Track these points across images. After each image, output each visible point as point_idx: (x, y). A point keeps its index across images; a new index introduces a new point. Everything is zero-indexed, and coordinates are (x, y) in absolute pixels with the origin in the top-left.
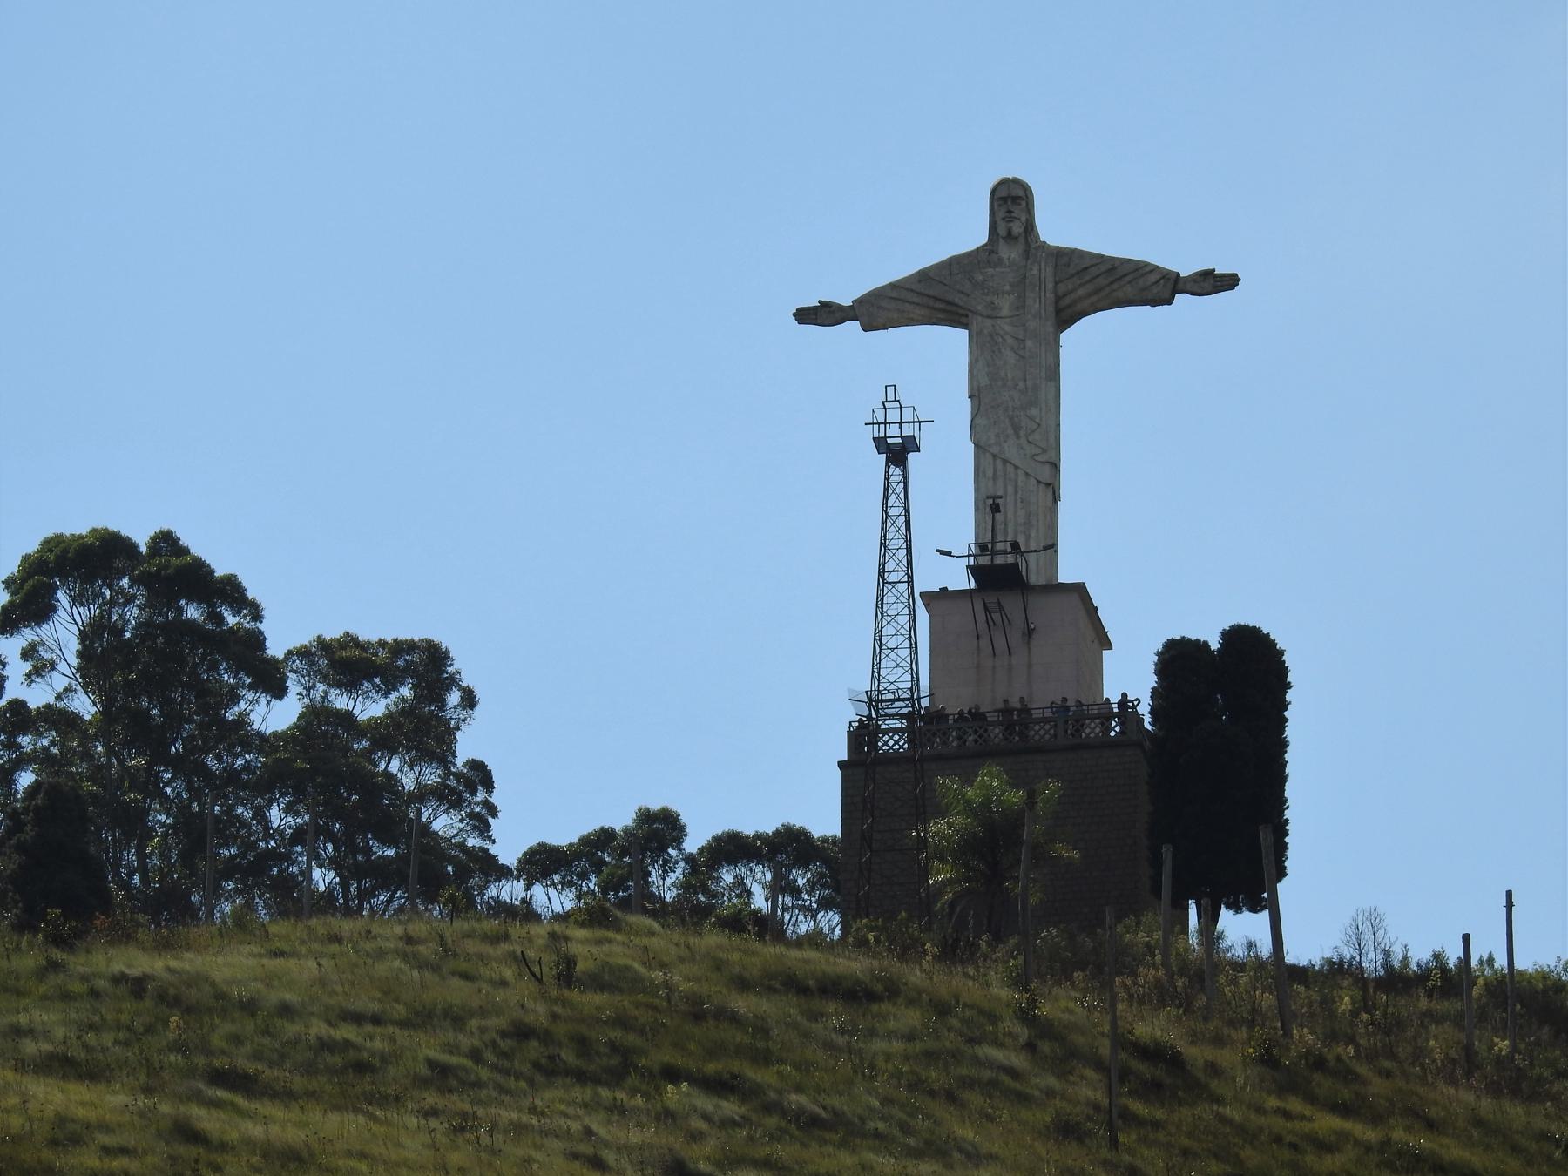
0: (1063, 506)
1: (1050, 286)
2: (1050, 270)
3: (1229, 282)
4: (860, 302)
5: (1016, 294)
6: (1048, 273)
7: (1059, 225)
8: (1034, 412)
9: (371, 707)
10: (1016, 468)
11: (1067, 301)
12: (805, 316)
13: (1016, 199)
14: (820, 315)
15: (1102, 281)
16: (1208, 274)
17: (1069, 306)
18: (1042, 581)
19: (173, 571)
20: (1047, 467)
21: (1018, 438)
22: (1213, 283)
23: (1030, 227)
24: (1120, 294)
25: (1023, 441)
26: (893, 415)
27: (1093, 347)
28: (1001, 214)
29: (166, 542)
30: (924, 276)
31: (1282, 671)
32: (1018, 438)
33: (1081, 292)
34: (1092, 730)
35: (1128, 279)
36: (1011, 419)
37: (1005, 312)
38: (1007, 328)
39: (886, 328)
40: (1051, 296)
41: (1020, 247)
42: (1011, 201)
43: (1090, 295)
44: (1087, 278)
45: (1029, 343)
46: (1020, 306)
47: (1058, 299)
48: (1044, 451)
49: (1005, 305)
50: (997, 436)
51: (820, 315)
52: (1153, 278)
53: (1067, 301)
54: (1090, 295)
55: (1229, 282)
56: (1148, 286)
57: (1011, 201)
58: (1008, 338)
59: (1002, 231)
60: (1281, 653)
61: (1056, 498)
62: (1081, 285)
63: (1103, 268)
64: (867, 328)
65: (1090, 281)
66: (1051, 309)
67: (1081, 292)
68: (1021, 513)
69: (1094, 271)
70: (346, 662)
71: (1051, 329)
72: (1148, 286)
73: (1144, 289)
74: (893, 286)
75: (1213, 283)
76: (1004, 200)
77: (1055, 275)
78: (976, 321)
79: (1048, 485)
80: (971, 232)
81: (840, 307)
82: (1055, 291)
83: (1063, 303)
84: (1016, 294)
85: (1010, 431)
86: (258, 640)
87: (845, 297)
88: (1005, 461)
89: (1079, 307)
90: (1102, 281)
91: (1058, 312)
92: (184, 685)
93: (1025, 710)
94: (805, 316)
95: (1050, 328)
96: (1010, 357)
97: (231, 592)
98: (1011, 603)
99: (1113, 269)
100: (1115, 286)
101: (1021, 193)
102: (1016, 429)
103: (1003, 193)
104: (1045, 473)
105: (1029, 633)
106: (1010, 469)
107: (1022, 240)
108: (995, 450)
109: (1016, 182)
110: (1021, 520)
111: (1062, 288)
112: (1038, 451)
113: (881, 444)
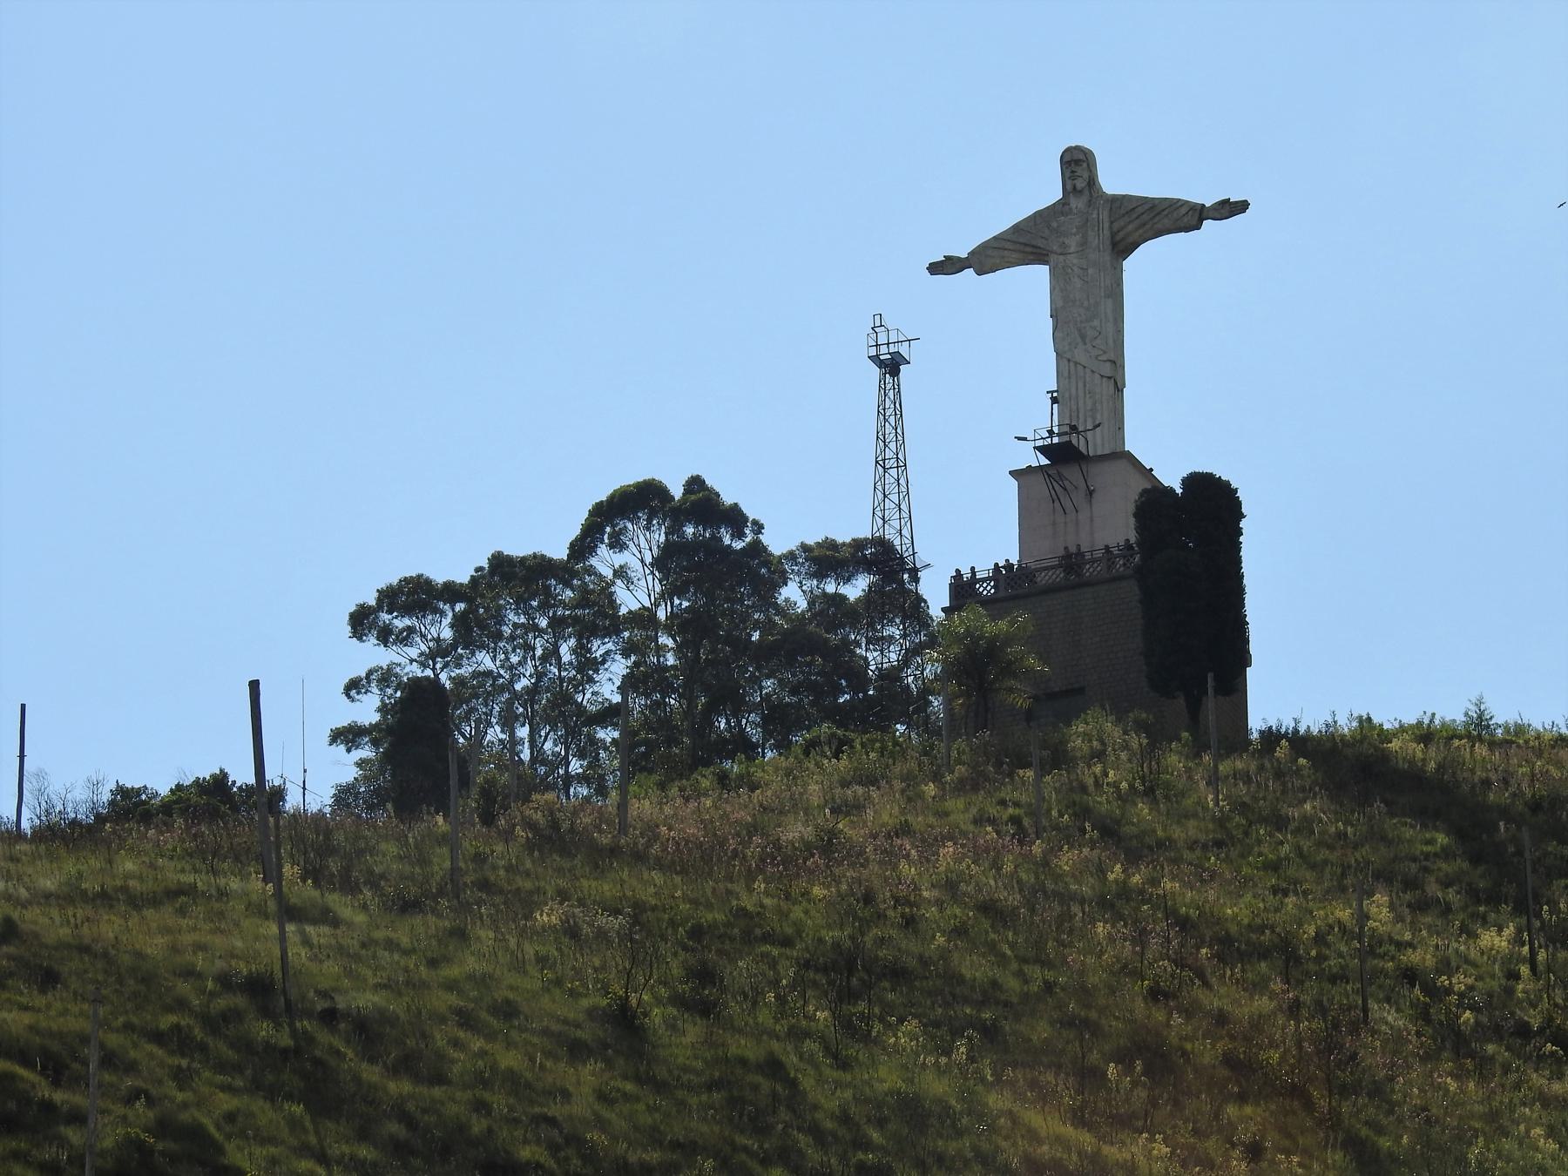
0: (1127, 393)
1: (1107, 225)
2: (1106, 213)
3: (1242, 207)
4: (972, 253)
5: (1087, 236)
6: (1105, 215)
7: (1113, 181)
8: (1096, 323)
9: (856, 589)
11: (1121, 234)
12: (935, 269)
13: (1077, 162)
14: (946, 266)
16: (1226, 202)
19: (703, 503)
22: (1230, 209)
23: (1092, 182)
24: (1159, 226)
25: (1089, 346)
26: (882, 339)
27: (1150, 269)
28: (1068, 174)
29: (695, 484)
30: (1017, 228)
31: (1237, 504)
33: (1130, 227)
34: (1088, 571)
37: (1072, 250)
40: (1107, 232)
41: (1085, 198)
42: (1077, 163)
43: (1137, 229)
45: (1090, 271)
46: (1084, 243)
49: (1073, 243)
51: (946, 266)
52: (1183, 210)
53: (1121, 234)
54: (1137, 229)
55: (1242, 207)
56: (1183, 217)
57: (1077, 163)
59: (1069, 187)
60: (1236, 491)
61: (1119, 388)
66: (1108, 242)
67: (1130, 227)
69: (1140, 210)
70: (827, 559)
71: (1108, 258)
72: (1183, 217)
75: (1230, 209)
76: (1069, 163)
78: (1053, 258)
80: (1049, 190)
83: (1118, 238)
84: (1087, 236)
86: (757, 549)
88: (1076, 363)
89: (1131, 240)
91: (1114, 245)
93: (1080, 554)
94: (935, 269)
95: (1107, 257)
96: (1078, 283)
97: (735, 518)
98: (1072, 473)
101: (1081, 157)
102: (1083, 337)
103: (1067, 158)
104: (1107, 369)
105: (1091, 493)
107: (1087, 192)
108: (1068, 355)
109: (1078, 148)
111: (1116, 226)
113: (875, 359)
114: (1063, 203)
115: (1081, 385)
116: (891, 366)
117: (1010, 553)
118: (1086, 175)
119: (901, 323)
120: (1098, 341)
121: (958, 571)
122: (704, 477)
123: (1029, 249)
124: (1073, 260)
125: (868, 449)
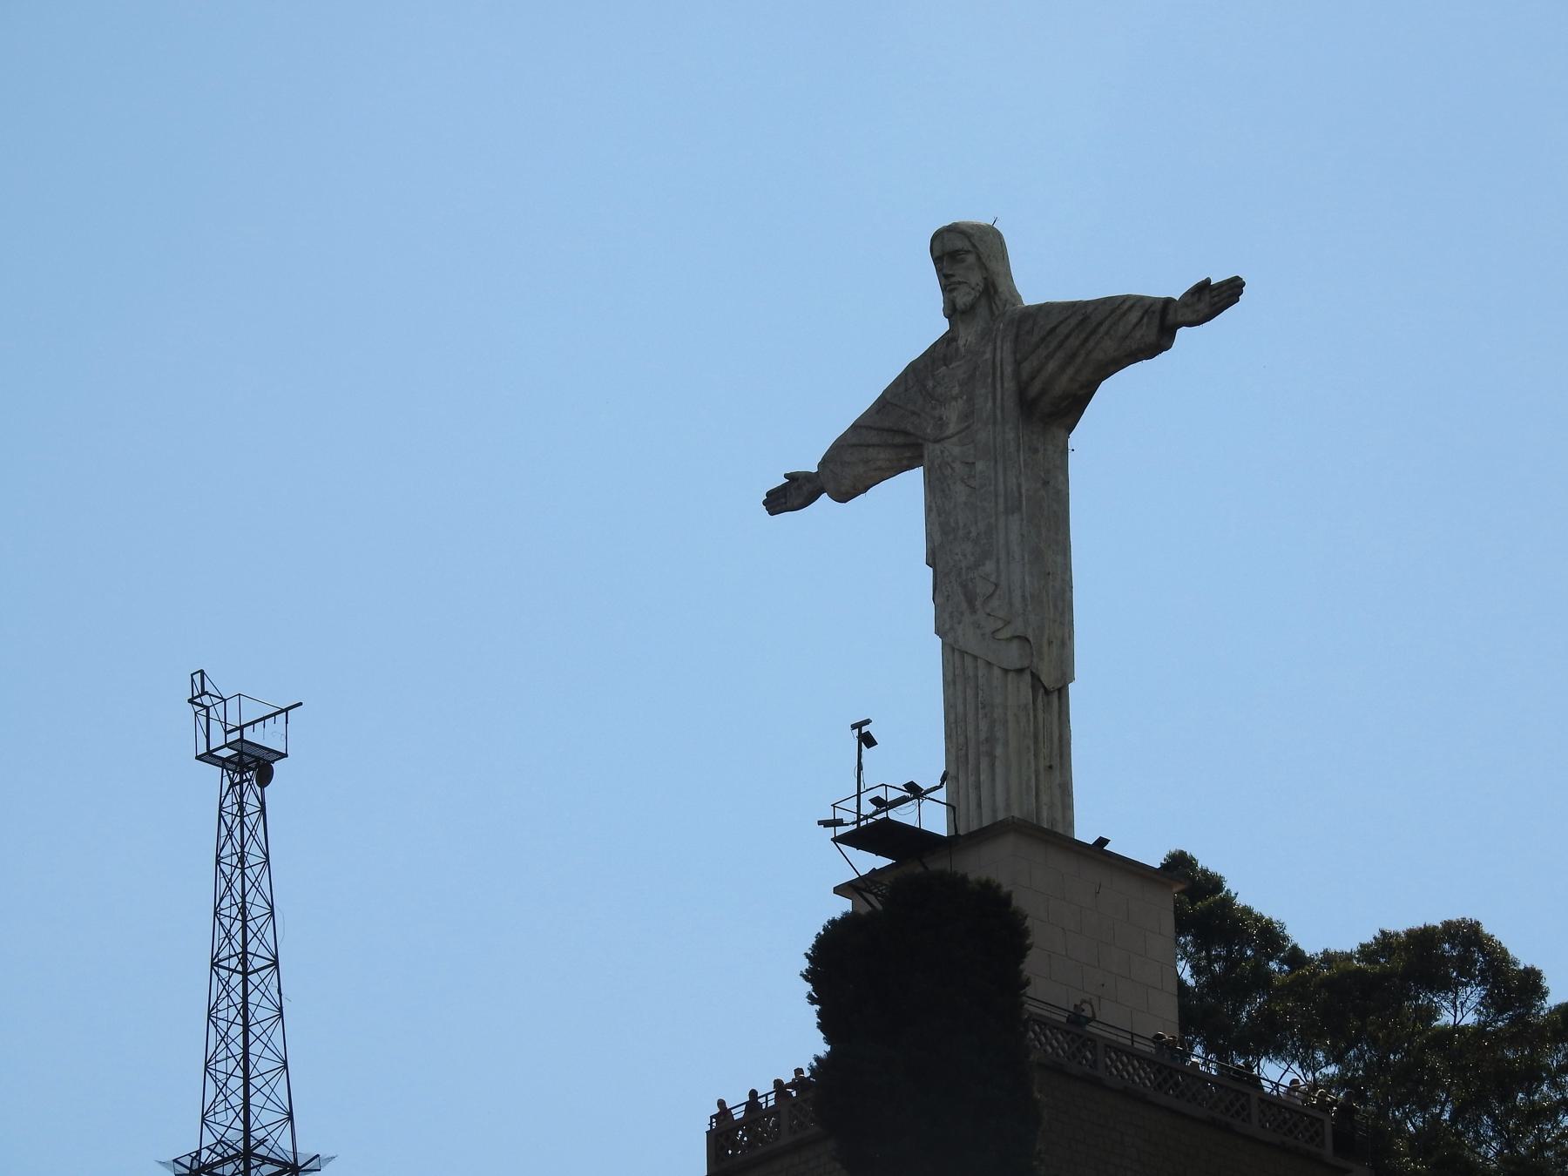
1: (1009, 370)
2: (1008, 346)
5: (997, 398)
6: (1005, 352)
7: (1041, 277)
8: (989, 566)
10: (975, 658)
11: (1036, 386)
15: (1074, 342)
16: (1203, 288)
17: (1043, 392)
18: (974, 827)
20: (1015, 644)
21: (974, 611)
22: (1214, 298)
27: (1120, 434)
32: (974, 611)
33: (1052, 366)
35: (1103, 329)
36: (964, 586)
38: (956, 450)
39: (865, 490)
40: (1010, 385)
42: (966, 257)
43: (1062, 369)
44: (1053, 345)
45: (980, 466)
47: (1021, 392)
48: (1007, 623)
50: (951, 617)
52: (1134, 317)
54: (1062, 369)
56: (1144, 328)
57: (966, 257)
58: (957, 465)
62: (1050, 357)
63: (1073, 322)
64: (842, 497)
65: (1060, 345)
67: (1052, 366)
68: (983, 726)
69: (1064, 330)
72: (1144, 328)
73: (1125, 337)
74: (856, 427)
75: (1214, 298)
77: (1015, 353)
78: (931, 450)
79: (1020, 671)
81: (807, 476)
82: (1017, 373)
84: (997, 398)
85: (964, 605)
87: (809, 463)
90: (1074, 342)
92: (1230, 952)
99: (1086, 319)
100: (1091, 344)
101: (966, 245)
102: (971, 601)
106: (968, 661)
110: (983, 736)
111: (1027, 368)
112: (1000, 624)
114: (947, 340)
115: (970, 692)
116: (250, 765)
117: (823, 1049)
118: (976, 278)
119: (249, 689)
120: (995, 603)
121: (753, 1093)
122: (1190, 851)
123: (899, 440)
124: (954, 448)
125: (196, 937)
